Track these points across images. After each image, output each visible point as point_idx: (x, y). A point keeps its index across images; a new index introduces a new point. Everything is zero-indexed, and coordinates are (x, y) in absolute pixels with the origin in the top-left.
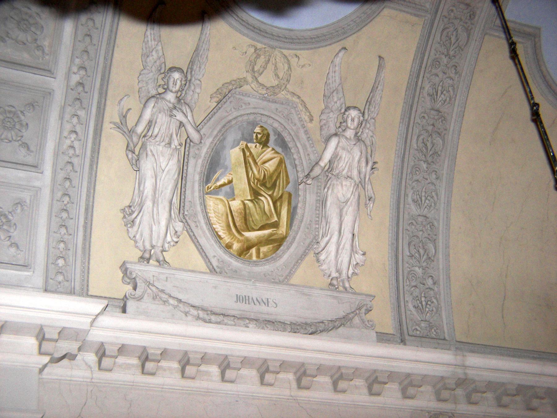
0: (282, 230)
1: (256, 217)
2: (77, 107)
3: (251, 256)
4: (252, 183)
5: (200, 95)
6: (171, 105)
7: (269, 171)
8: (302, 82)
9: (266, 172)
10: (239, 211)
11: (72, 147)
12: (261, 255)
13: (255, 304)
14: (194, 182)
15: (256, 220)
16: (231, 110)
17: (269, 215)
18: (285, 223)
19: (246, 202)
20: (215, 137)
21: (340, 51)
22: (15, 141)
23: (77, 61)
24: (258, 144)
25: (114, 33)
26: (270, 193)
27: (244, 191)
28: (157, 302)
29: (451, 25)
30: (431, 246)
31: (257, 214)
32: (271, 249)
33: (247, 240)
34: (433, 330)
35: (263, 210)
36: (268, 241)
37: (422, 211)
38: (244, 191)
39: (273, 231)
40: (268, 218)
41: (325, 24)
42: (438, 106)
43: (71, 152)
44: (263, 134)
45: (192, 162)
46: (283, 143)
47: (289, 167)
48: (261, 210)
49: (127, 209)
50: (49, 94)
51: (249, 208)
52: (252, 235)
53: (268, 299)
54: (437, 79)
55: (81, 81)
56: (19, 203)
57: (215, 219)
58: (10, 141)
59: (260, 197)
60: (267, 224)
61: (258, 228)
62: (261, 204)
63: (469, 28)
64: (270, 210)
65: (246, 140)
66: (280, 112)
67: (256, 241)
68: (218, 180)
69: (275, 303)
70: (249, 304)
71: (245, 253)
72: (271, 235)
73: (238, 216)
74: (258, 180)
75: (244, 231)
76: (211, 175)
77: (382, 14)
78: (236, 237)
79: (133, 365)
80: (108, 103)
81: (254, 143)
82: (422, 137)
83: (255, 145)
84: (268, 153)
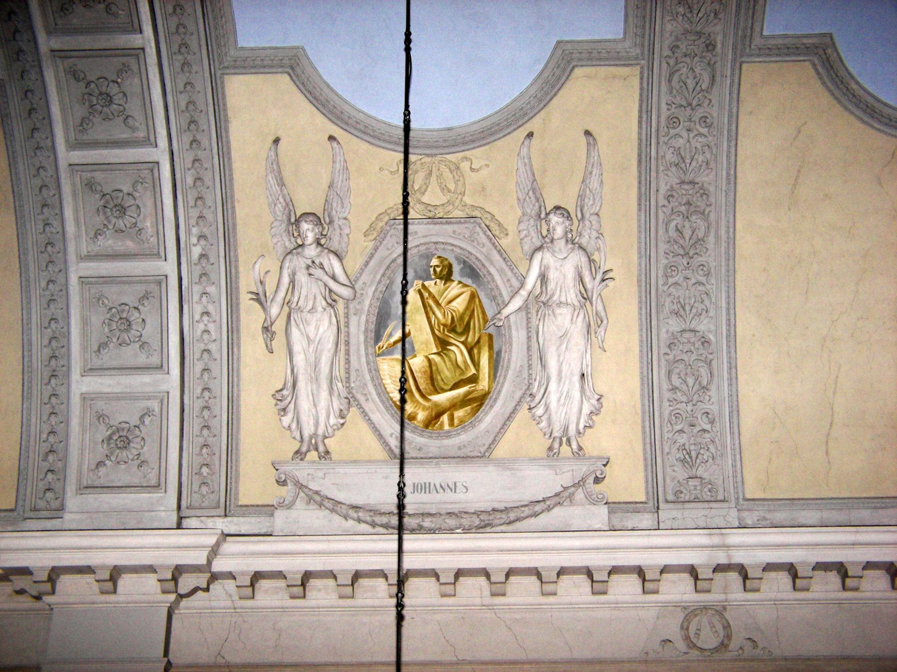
0: (484, 384)
1: (447, 373)
2: (204, 284)
3: (442, 425)
4: (436, 332)
5: (350, 236)
6: (309, 262)
7: (458, 311)
8: (484, 189)
9: (454, 314)
10: (423, 370)
11: (206, 331)
12: (456, 421)
13: (437, 492)
14: (359, 345)
15: (447, 377)
16: (393, 246)
17: (463, 367)
18: (487, 375)
19: (431, 357)
20: (380, 282)
22: (134, 342)
23: (195, 230)
24: (438, 281)
26: (463, 339)
27: (427, 343)
28: (311, 507)
29: (681, 65)
30: (704, 372)
31: (447, 369)
32: (469, 411)
33: (436, 405)
34: (706, 490)
35: (454, 362)
36: (464, 402)
37: (688, 323)
38: (427, 343)
39: (470, 388)
40: (463, 373)
41: (497, 109)
42: (690, 177)
43: (206, 336)
44: (443, 266)
45: (353, 320)
46: (472, 272)
47: (485, 302)
48: (452, 364)
50: (161, 281)
51: (436, 364)
52: (442, 398)
53: (455, 484)
54: (681, 141)
55: (204, 252)
56: (148, 412)
57: (392, 386)
58: (129, 345)
59: (449, 347)
60: (462, 380)
61: (450, 387)
62: (452, 355)
63: (712, 62)
64: (465, 362)
65: (420, 278)
66: (459, 234)
67: (448, 404)
68: (390, 335)
69: (465, 487)
70: (430, 492)
71: (434, 422)
72: (469, 393)
73: (421, 377)
74: (445, 325)
75: (431, 395)
76: (382, 333)
77: (574, 75)
78: (421, 404)
80: (241, 269)
81: (432, 279)
82: (673, 225)
83: (434, 281)
84: (453, 289)
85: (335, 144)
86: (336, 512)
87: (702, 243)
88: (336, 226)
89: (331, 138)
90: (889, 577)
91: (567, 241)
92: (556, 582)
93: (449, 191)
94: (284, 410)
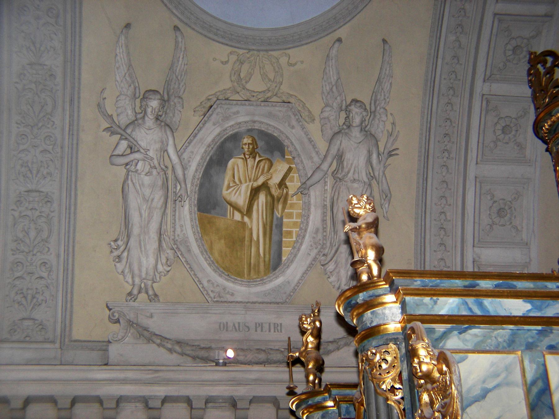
21: (334, 43)
25: (76, 89)
49: (112, 243)
79: (301, 372)
85: (178, 33)
86: (163, 346)
87: (50, 117)
88: (172, 103)
89: (176, 28)
90: (276, 409)
91: (361, 130)
92: (204, 409)
93: (270, 80)
94: (119, 257)
